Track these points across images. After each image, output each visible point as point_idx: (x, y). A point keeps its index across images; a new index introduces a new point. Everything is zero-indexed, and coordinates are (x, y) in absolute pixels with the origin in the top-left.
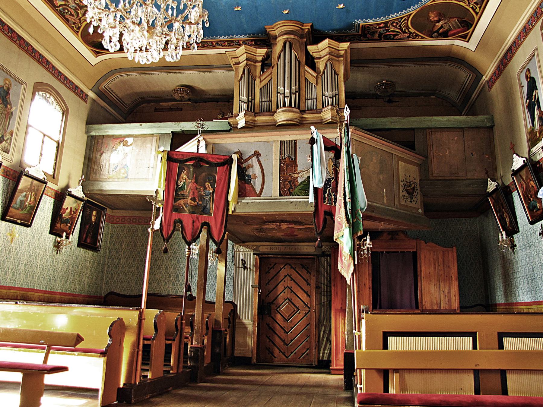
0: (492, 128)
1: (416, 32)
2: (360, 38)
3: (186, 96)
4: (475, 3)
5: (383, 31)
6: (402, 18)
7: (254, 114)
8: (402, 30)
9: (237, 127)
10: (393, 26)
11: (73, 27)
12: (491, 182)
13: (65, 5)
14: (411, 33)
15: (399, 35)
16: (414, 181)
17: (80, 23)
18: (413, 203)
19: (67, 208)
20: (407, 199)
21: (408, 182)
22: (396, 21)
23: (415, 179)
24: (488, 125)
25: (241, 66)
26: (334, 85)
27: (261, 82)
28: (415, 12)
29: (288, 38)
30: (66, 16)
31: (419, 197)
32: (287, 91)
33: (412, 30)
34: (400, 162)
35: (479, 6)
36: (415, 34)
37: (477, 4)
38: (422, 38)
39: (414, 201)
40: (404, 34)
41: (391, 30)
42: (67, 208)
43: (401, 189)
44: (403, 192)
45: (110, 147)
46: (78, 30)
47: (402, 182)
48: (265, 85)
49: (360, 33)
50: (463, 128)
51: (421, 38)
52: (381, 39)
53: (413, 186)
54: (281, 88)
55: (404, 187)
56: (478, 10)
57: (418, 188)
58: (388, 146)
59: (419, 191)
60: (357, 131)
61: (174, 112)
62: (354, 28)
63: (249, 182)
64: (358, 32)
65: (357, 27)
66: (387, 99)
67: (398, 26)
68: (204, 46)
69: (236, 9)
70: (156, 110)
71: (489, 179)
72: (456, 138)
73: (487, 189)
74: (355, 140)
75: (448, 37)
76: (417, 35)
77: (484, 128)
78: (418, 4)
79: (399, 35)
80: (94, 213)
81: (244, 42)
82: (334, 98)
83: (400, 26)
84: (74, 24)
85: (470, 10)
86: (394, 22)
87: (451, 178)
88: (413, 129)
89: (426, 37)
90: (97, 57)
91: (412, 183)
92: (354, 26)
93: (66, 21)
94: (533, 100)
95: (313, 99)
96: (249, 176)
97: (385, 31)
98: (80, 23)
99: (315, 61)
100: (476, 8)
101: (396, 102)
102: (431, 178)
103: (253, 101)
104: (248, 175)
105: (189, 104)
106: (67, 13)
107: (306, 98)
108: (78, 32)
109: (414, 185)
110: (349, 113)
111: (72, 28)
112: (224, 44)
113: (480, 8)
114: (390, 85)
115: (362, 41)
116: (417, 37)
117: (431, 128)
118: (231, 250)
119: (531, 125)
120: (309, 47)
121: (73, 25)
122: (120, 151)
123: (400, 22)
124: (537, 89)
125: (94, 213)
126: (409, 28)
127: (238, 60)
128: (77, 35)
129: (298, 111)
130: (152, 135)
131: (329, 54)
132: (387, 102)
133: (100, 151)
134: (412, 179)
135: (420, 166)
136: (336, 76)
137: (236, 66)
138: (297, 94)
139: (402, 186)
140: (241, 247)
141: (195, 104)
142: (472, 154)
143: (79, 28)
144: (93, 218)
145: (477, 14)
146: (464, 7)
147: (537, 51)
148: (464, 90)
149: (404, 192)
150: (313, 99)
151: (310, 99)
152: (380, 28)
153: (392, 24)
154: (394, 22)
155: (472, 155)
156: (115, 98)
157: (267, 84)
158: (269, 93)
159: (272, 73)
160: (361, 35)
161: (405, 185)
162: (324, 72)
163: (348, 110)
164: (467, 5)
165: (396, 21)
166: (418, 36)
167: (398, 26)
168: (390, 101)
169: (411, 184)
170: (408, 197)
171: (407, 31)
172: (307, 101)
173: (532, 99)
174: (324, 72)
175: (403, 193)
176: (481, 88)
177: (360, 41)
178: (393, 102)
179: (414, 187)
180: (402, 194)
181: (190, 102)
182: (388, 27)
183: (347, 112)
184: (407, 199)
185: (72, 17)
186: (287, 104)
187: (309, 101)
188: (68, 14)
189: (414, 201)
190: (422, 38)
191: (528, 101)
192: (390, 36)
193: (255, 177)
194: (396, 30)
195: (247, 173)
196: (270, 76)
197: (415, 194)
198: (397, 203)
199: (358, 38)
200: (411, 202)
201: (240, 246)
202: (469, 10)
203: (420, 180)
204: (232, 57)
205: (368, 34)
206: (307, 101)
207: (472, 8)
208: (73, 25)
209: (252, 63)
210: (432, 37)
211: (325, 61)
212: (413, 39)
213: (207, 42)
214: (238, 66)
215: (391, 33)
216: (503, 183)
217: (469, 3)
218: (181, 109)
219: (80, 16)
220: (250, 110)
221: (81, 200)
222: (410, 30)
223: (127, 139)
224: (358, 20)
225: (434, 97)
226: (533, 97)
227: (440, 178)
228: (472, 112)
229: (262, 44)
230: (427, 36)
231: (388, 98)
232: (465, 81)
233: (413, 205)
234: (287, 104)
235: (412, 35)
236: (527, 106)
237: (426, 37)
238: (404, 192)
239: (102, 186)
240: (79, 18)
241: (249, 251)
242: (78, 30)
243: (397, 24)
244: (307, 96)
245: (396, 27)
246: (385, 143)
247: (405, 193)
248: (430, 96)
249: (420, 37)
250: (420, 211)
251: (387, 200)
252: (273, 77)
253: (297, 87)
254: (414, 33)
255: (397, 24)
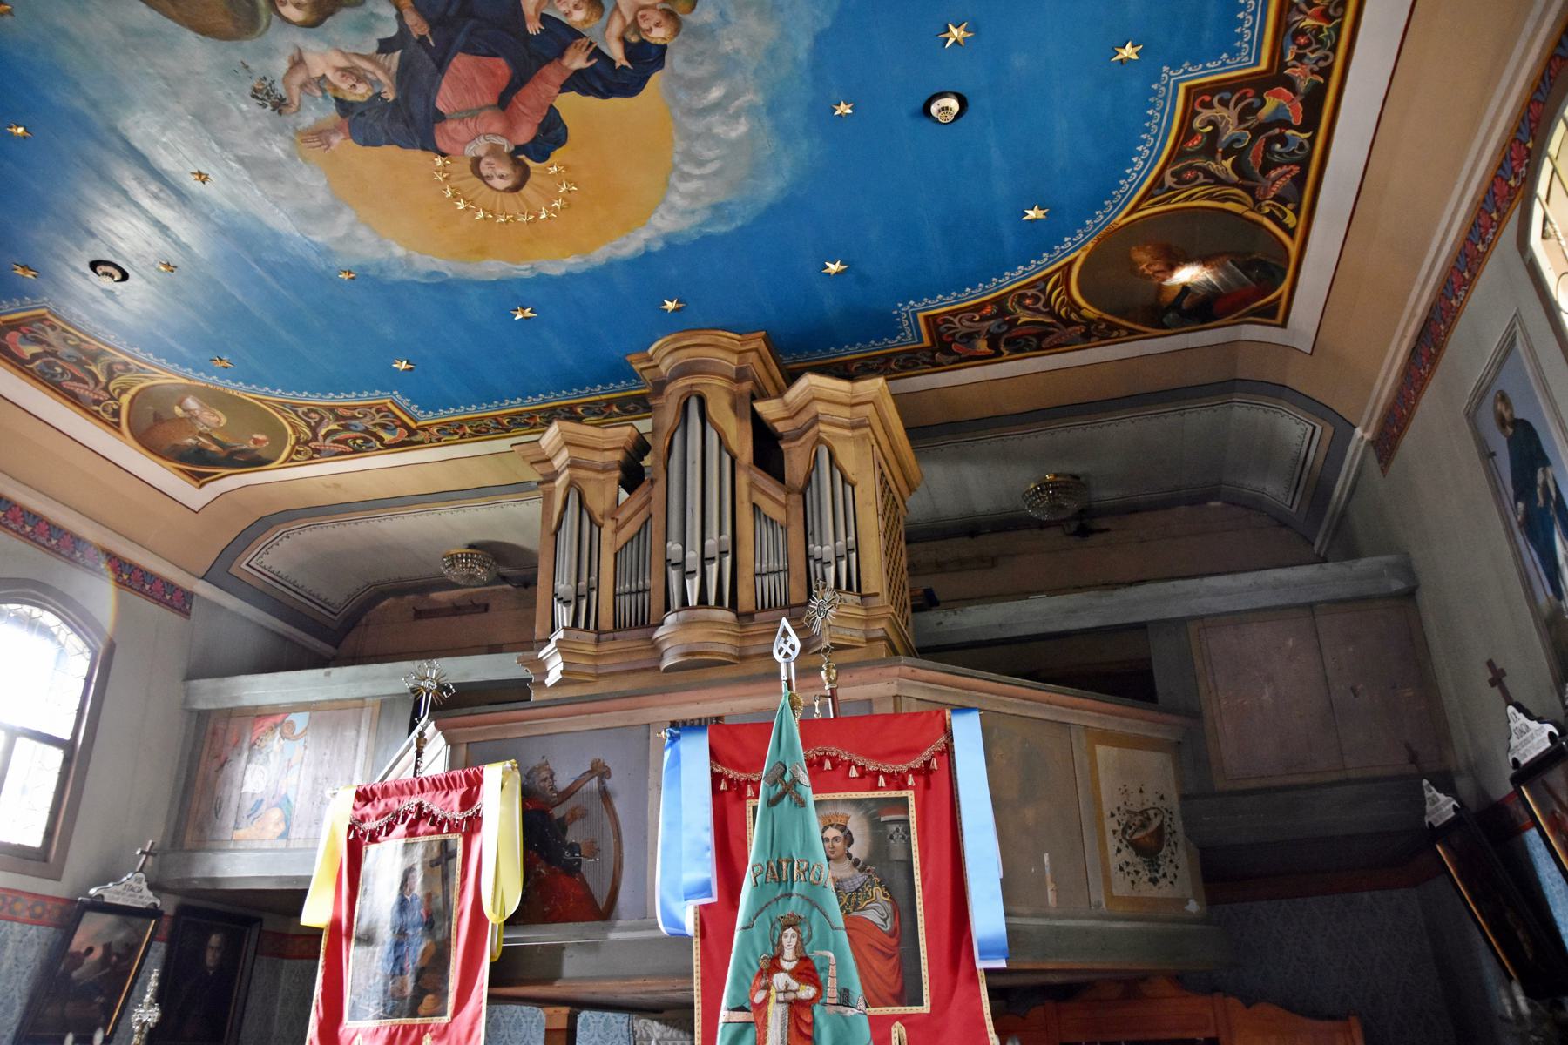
0: (1410, 594)
1: (1106, 316)
2: (933, 357)
3: (480, 572)
4: (1275, 198)
5: (999, 327)
6: (1046, 279)
7: (593, 636)
8: (1058, 317)
9: (543, 683)
10: (1027, 308)
11: (98, 412)
12: (1435, 792)
13: (46, 353)
14: (1089, 322)
15: (1053, 333)
16: (1159, 804)
17: (112, 398)
18: (1163, 882)
19: (90, 950)
20: (1137, 872)
21: (1135, 814)
22: (1030, 292)
23: (1162, 798)
24: (1397, 585)
25: (560, 485)
26: (641, 563)
27: (617, 531)
28: (1081, 255)
29: (692, 385)
30: (65, 385)
31: (1182, 857)
32: (693, 556)
33: (1090, 312)
34: (1100, 750)
35: (1290, 206)
36: (1103, 326)
37: (1285, 203)
38: (1131, 332)
39: (1164, 875)
40: (1070, 329)
41: (1023, 319)
42: (90, 950)
43: (1112, 843)
44: (1119, 851)
45: (246, 745)
46: (116, 420)
47: (1112, 815)
48: (632, 540)
49: (927, 342)
50: (1310, 606)
51: (1129, 334)
52: (999, 354)
53: (1156, 823)
54: (674, 547)
55: (1124, 832)
56: (1290, 219)
57: (1178, 825)
58: (1048, 703)
59: (1180, 836)
60: (919, 671)
61: (465, 618)
62: (903, 330)
63: (573, 869)
64: (921, 341)
65: (910, 325)
66: (1073, 526)
67: (1040, 305)
68: (480, 432)
69: (519, 317)
70: (419, 614)
71: (1425, 782)
72: (1290, 643)
73: (1424, 813)
74: (918, 699)
75: (1216, 319)
76: (1112, 327)
77: (1382, 597)
78: (1085, 226)
79: (1053, 333)
80: (215, 940)
81: (588, 408)
82: (854, 554)
83: (1047, 303)
84: (97, 402)
85: (1267, 222)
86: (1023, 296)
87: (1290, 780)
88: (1141, 627)
89: (1143, 329)
90: (202, 486)
91: (1151, 813)
92: (901, 323)
93: (73, 399)
94: (1541, 501)
95: (779, 571)
96: (574, 848)
97: (1005, 328)
98: (112, 398)
99: (783, 446)
100: (1285, 215)
101: (1101, 531)
102: (1220, 784)
103: (594, 593)
104: (572, 844)
105: (506, 590)
106: (62, 374)
107: (758, 570)
108: (118, 424)
109: (1159, 818)
110: (794, 655)
111: (95, 415)
112: (532, 422)
113: (1296, 212)
114: (1072, 484)
115: (940, 365)
116: (1116, 333)
117: (1201, 618)
118: (626, 1034)
119: (1550, 594)
120: (760, 406)
121: (96, 408)
122: (271, 756)
123: (1043, 291)
124: (1545, 462)
125: (215, 940)
126: (1080, 308)
127: (552, 466)
128: (120, 432)
129: (730, 616)
130: (360, 703)
131: (567, 444)
132: (1074, 534)
133: (218, 757)
134: (1150, 800)
135: (1176, 749)
136: (596, 530)
137: (545, 486)
138: (728, 560)
139: (1114, 832)
140: (656, 1024)
141: (523, 590)
142: (1353, 690)
143: (116, 413)
144: (211, 958)
145: (1291, 233)
146: (1240, 216)
147: (1524, 329)
148: (1304, 477)
149: (1124, 852)
150: (779, 571)
151: (769, 573)
152: (983, 319)
153: (1020, 303)
154: (1023, 296)
155: (1356, 696)
156: (89, 630)
157: (639, 533)
158: (642, 566)
159: (651, 498)
160: (932, 350)
161: (1128, 826)
162: (808, 481)
163: (794, 639)
164: (1252, 210)
165: (1030, 292)
166: (1118, 327)
167: (1040, 305)
168: (1084, 532)
169: (1149, 819)
170: (1139, 868)
171: (1073, 316)
172: (759, 580)
173: (1537, 501)
174: (808, 481)
175: (1118, 855)
176: (1351, 477)
177: (936, 366)
178: (1092, 532)
179: (1160, 827)
180: (1114, 861)
181: (508, 586)
182: (1013, 314)
183: (787, 649)
184: (1137, 872)
185: (81, 385)
186: (693, 599)
187: (766, 579)
188: (65, 377)
189: (1164, 875)
190: (1131, 332)
191: (1521, 505)
192: (1027, 340)
193: (594, 851)
194: (1040, 319)
195: (571, 838)
196: (645, 509)
197: (1165, 850)
198: (1098, 895)
199: (925, 359)
200: (1154, 881)
201: (653, 1020)
202: (1261, 225)
203: (1184, 798)
204: (533, 459)
205: (954, 341)
206: (759, 580)
207: (1271, 216)
208: (96, 408)
209: (591, 474)
210: (1165, 327)
211: (809, 445)
212: (1101, 339)
213: (482, 419)
214: (551, 485)
215: (1025, 329)
216: (1482, 793)
217: (1256, 201)
218: (486, 608)
219: (103, 379)
220: (582, 624)
221: (151, 913)
222: (1084, 312)
223: (292, 717)
224: (906, 304)
225: (1218, 504)
226: (1539, 490)
227: (1253, 784)
228: (1344, 546)
229: (641, 410)
230: (1144, 324)
231: (1078, 522)
232: (1304, 451)
233: (1164, 890)
234: (693, 599)
235: (1097, 328)
236: (1521, 525)
237: (1143, 329)
238: (1124, 852)
239: (213, 869)
240: (101, 386)
241: (678, 1039)
242: (116, 420)
243: (1037, 299)
244: (758, 565)
245: (1037, 311)
246: (1033, 693)
247: (1128, 855)
248: (1205, 503)
249: (1124, 332)
250: (1193, 907)
251: (1057, 891)
252: (653, 511)
253: (727, 535)
254: (1101, 319)
255: (1037, 299)
